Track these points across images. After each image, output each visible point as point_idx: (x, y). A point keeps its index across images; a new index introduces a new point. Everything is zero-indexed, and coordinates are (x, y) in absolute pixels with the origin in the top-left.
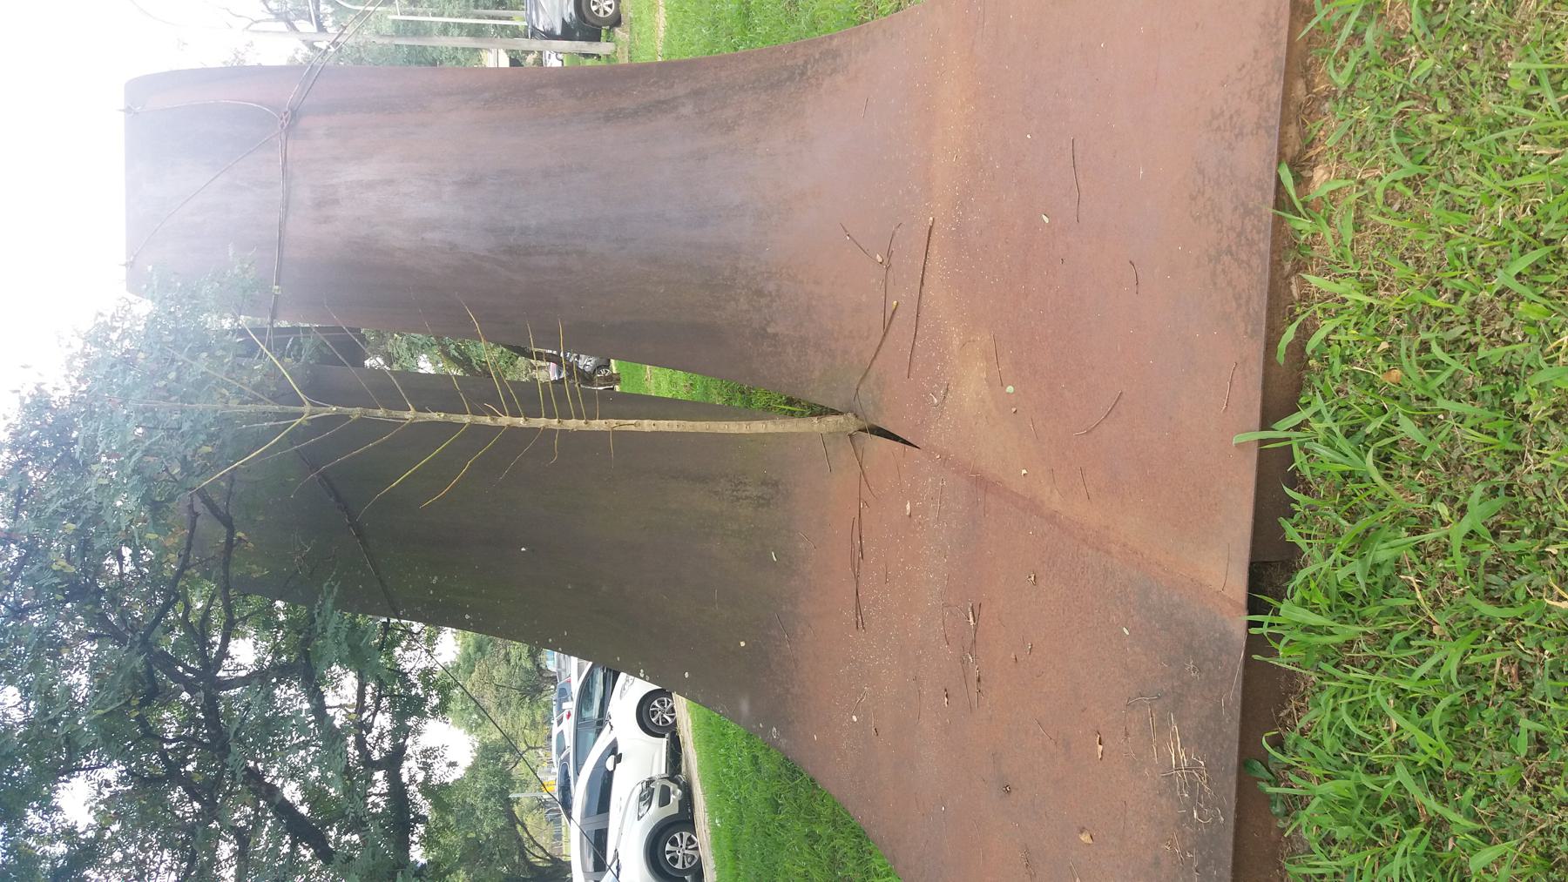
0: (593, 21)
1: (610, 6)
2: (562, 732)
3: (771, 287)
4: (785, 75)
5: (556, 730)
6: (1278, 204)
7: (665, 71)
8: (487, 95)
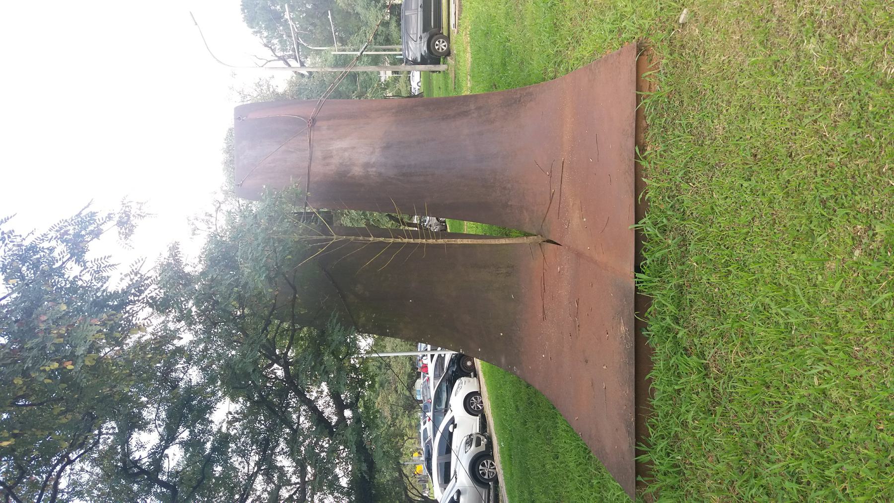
0: (436, 54)
1: (445, 46)
2: (426, 428)
3: (509, 186)
4: (513, 101)
5: (423, 428)
8: (393, 110)
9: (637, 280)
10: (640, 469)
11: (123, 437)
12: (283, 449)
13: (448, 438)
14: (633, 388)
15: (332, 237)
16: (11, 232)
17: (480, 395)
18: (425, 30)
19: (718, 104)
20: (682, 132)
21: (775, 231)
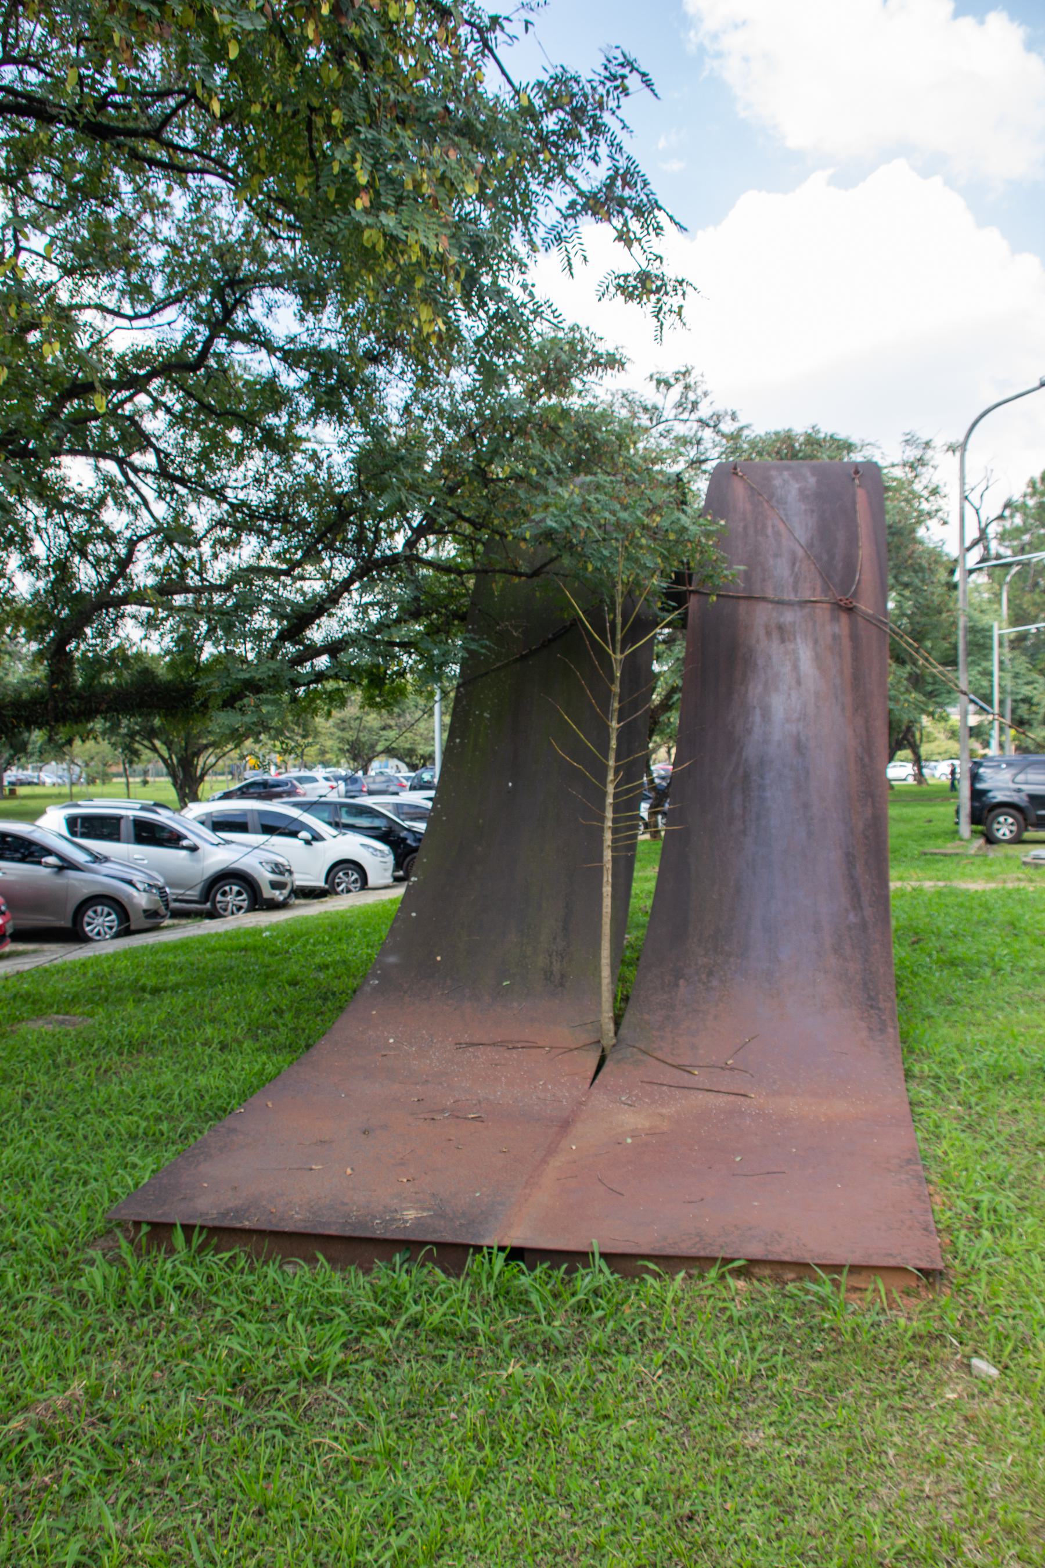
0: (991, 817)
3: (715, 983)
4: (872, 994)
6: (723, 1259)
7: (882, 898)
10: (161, 1230)
13: (288, 829)
14: (301, 1228)
15: (618, 651)
16: (625, 92)
18: (1033, 798)
19: (804, 1437)
20: (763, 1356)
21: (541, 1555)
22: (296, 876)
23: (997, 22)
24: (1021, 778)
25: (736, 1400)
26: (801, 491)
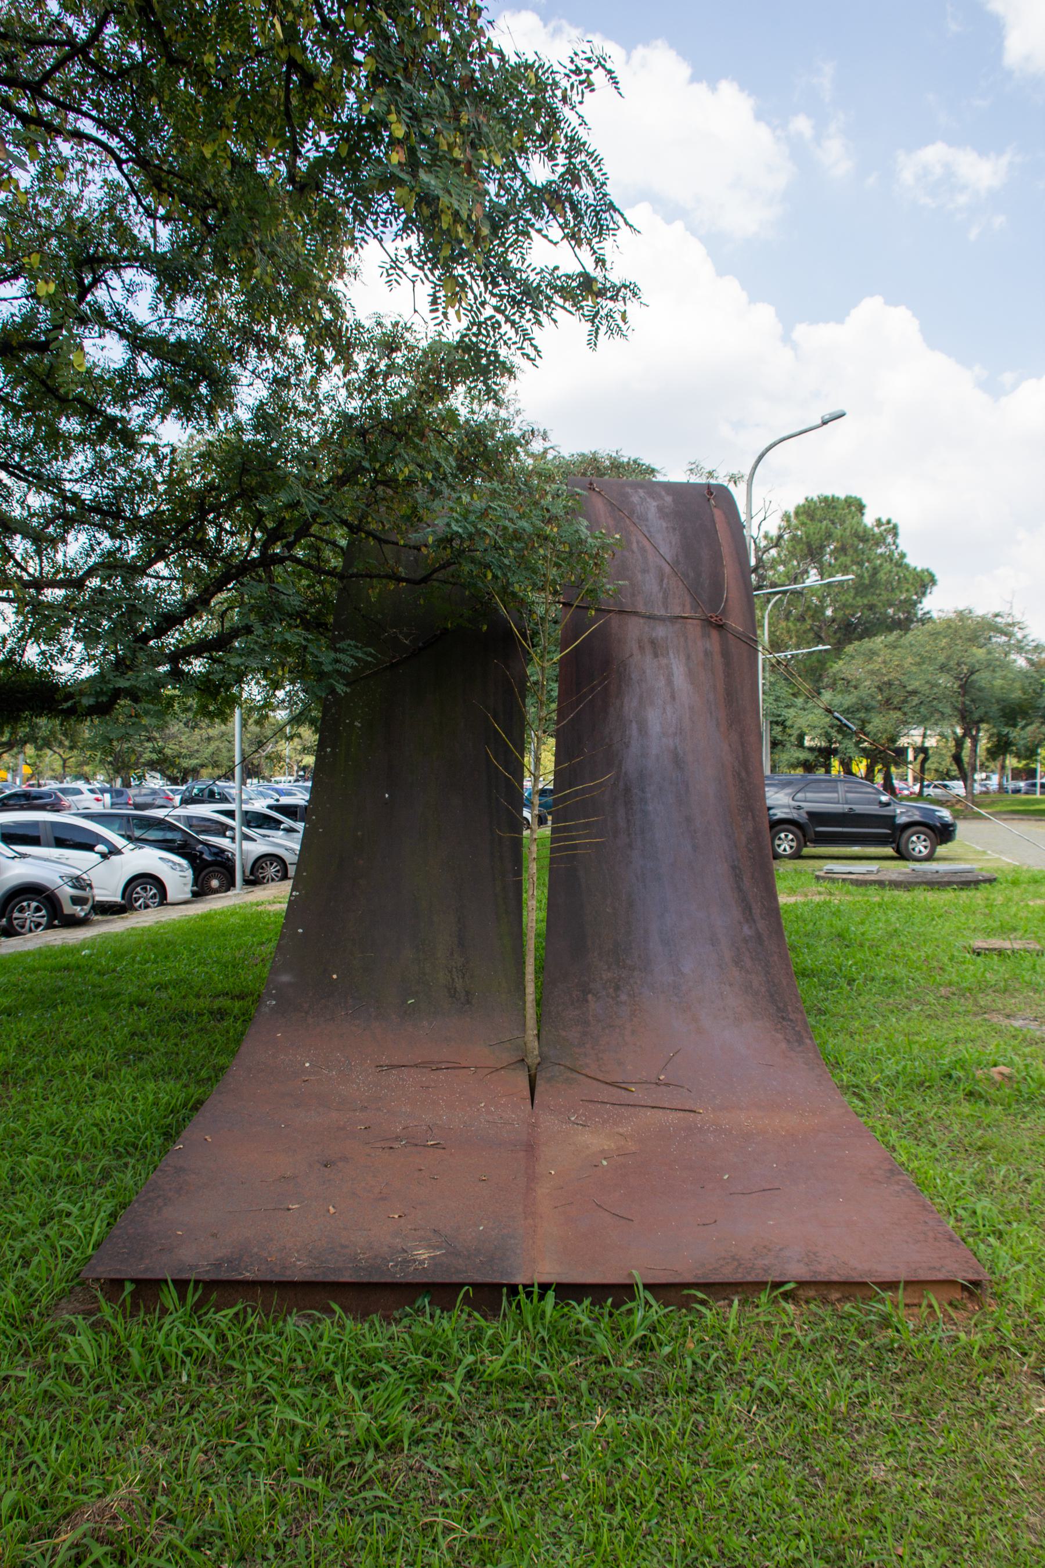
3: (624, 997)
4: (781, 1005)
7: (773, 911)
9: (536, 1289)
11: (148, 260)
12: (99, 544)
13: (85, 843)
14: (309, 1276)
16: (591, 86)
17: (161, 904)
18: (811, 815)
22: (96, 891)
23: (727, 89)
24: (800, 796)
25: (841, 1432)
26: (660, 509)
